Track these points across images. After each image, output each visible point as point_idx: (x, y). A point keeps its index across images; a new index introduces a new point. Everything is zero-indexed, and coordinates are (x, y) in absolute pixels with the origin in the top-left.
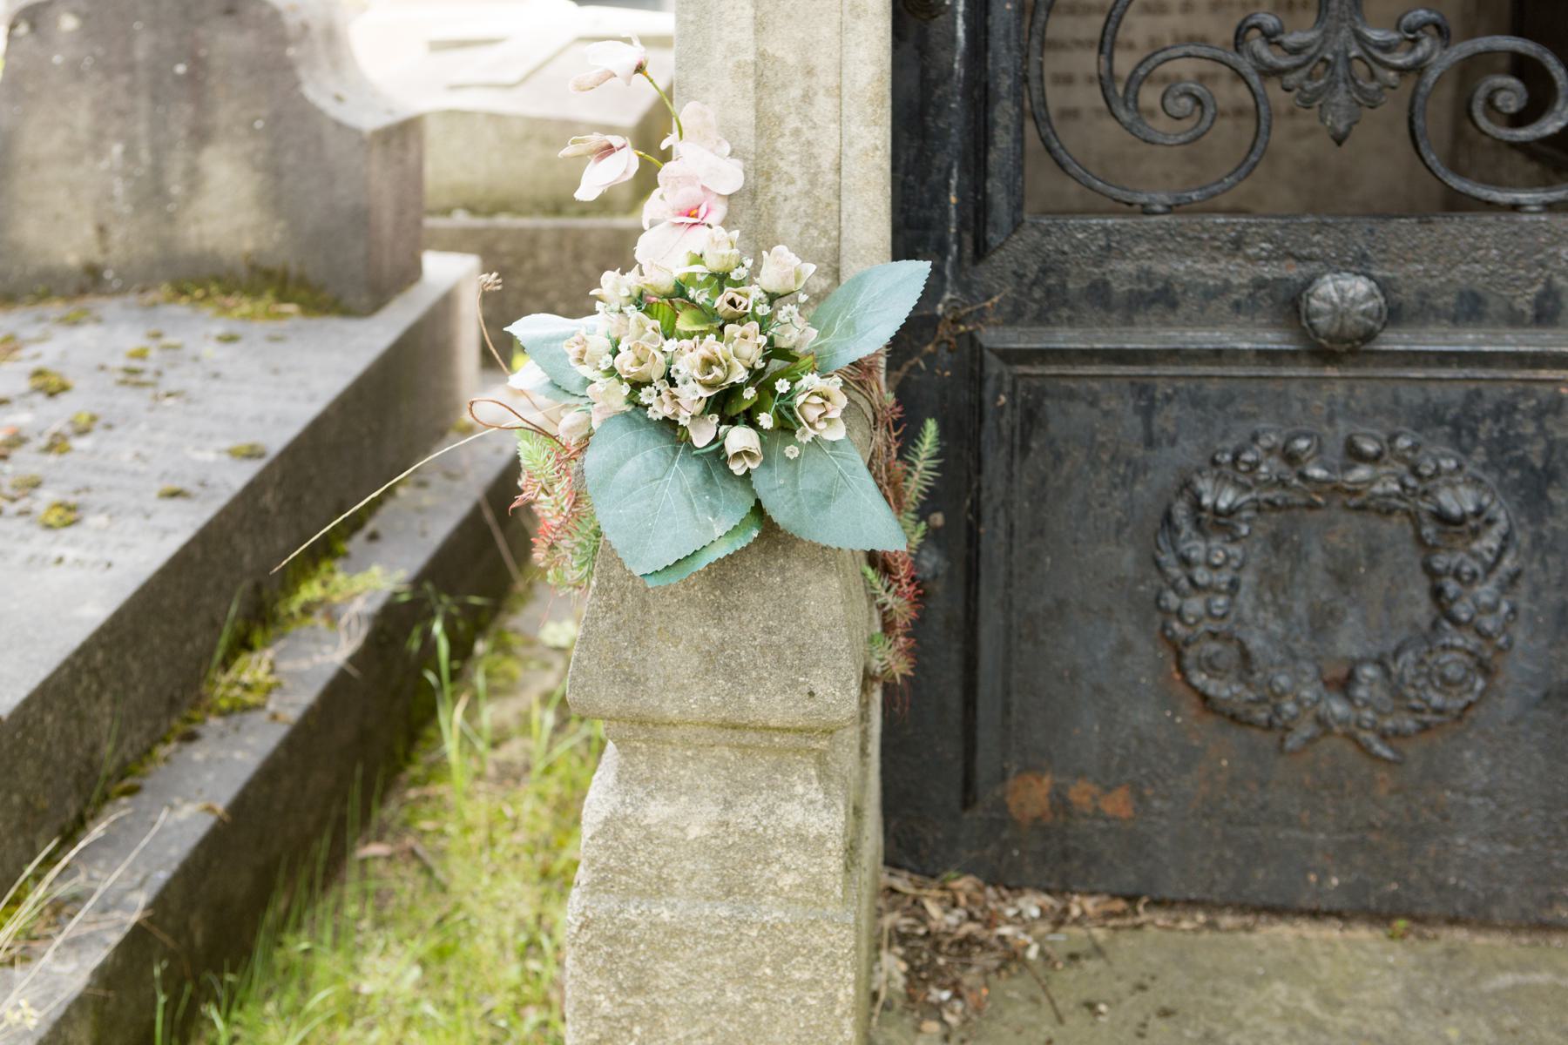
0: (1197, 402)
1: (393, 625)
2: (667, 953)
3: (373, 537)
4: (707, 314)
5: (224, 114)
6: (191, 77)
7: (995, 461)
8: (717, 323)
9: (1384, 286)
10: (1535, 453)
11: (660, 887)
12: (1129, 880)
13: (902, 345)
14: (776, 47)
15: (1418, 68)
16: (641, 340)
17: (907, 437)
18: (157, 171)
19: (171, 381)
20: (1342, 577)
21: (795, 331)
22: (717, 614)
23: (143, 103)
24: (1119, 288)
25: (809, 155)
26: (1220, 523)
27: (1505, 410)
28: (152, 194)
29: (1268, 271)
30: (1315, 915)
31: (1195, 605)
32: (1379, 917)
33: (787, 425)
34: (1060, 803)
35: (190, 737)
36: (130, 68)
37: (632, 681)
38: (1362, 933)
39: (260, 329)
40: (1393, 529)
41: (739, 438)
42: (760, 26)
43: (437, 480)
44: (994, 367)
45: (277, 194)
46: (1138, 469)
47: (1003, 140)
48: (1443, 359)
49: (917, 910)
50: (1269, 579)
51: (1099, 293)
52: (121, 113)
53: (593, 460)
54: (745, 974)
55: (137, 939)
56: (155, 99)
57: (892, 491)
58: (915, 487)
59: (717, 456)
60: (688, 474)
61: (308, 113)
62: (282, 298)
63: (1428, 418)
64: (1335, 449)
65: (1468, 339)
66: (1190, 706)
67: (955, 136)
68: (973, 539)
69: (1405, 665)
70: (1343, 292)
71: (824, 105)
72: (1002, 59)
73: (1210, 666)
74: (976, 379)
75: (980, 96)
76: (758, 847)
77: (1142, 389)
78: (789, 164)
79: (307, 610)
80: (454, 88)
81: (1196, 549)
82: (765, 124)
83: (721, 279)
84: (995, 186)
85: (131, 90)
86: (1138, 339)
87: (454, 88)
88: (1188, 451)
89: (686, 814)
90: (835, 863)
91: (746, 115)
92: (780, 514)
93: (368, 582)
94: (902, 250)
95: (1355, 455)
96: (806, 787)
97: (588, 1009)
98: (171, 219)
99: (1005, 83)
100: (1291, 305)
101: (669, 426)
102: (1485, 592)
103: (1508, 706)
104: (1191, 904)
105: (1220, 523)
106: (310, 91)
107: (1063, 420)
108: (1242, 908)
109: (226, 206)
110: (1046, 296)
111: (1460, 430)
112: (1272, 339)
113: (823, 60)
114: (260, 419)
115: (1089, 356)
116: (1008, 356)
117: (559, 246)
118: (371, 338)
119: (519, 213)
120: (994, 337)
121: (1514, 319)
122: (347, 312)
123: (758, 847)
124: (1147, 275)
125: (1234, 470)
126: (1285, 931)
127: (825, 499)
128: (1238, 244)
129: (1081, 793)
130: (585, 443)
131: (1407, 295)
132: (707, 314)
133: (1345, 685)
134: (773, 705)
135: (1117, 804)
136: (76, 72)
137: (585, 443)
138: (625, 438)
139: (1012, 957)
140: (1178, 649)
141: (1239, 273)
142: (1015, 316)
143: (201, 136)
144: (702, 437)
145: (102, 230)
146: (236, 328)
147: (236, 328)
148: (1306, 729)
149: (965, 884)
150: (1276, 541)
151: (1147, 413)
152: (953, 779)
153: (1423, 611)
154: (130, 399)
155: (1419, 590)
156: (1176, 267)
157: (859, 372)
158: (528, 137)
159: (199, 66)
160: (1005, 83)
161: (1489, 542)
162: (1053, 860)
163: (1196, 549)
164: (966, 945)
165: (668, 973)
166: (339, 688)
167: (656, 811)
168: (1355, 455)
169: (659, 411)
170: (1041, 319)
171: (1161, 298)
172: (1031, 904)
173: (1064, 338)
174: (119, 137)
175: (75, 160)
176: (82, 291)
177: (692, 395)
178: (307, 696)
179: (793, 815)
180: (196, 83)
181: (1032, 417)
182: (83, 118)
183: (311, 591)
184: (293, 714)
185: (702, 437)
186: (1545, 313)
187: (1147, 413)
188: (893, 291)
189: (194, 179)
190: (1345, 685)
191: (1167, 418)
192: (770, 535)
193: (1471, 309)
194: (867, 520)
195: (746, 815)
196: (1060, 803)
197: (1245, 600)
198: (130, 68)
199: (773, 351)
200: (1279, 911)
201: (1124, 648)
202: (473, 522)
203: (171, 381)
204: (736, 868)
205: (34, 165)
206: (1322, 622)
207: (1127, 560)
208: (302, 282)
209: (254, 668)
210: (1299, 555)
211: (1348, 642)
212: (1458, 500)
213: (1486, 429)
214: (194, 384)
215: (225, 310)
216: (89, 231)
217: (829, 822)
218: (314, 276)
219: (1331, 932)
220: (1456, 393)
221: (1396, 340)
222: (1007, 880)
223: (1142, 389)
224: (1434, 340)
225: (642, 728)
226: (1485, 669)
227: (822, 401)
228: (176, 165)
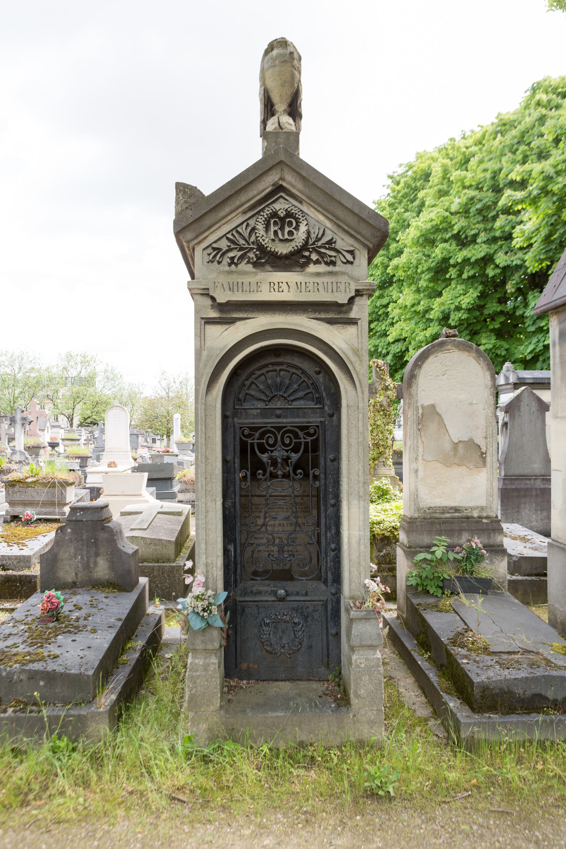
0: (264, 607)
1: (144, 651)
2: (198, 678)
3: (136, 636)
4: (201, 599)
5: (102, 550)
6: (94, 542)
7: (239, 617)
8: (203, 600)
9: (286, 591)
10: (306, 613)
11: (197, 671)
12: (257, 678)
13: (225, 601)
14: (209, 561)
15: (291, 560)
16: (194, 603)
17: (226, 614)
18: (88, 562)
19: (100, 606)
20: (283, 632)
21: (212, 600)
22: (203, 636)
23: (85, 547)
24: (254, 591)
25: (213, 576)
26: (267, 625)
27: (302, 608)
28: (87, 567)
29: (273, 589)
30: (281, 681)
31: (265, 637)
32: (289, 680)
33: (211, 612)
34: (249, 667)
35: (118, 668)
36: (82, 540)
37: (194, 645)
38: (287, 683)
39: (111, 595)
40: (289, 625)
41: (206, 614)
42: (206, 558)
43: (145, 625)
44: (238, 603)
45: (112, 567)
46: (257, 617)
47: (239, 570)
48: (294, 601)
49: (229, 683)
50: (274, 633)
51: (252, 592)
52: (80, 550)
53: (189, 617)
54: (207, 680)
55: (120, 693)
56: (87, 547)
57: (223, 621)
58: (227, 620)
59: (203, 616)
60: (199, 619)
61: (119, 550)
62: (114, 588)
63: (293, 609)
64: (282, 615)
65: (297, 598)
66: (265, 652)
67: (232, 569)
68: (236, 629)
69: (290, 644)
70: (282, 592)
71: (214, 568)
72: (238, 558)
73: (267, 645)
74: (236, 605)
75: (235, 564)
76: (208, 665)
77: (257, 606)
78: (210, 577)
79: (129, 648)
80: (132, 530)
81: (265, 628)
82: (207, 571)
83: (203, 595)
84: (238, 577)
85: (82, 545)
86: (257, 599)
87: (132, 530)
88: (263, 615)
89: (200, 661)
90: (217, 666)
91: (205, 570)
92: (210, 623)
93: (139, 643)
94: (225, 590)
95: (284, 615)
96: (214, 657)
97: (189, 686)
98: (91, 572)
99: (239, 562)
100: (275, 593)
101: (197, 613)
102: (300, 633)
103: (303, 649)
104: (265, 680)
105: (267, 625)
106: (119, 546)
107: (247, 610)
108: (272, 680)
109: (102, 569)
110: (245, 593)
111: (297, 611)
112: (273, 599)
113: (214, 562)
114: (119, 613)
115: (250, 601)
116: (240, 602)
117: (159, 570)
118: (133, 597)
119: (149, 562)
120: (239, 599)
121: (303, 595)
122: (127, 591)
123: (208, 665)
124: (257, 590)
125: (269, 617)
126: (277, 683)
127: (215, 621)
128: (269, 585)
129: (251, 665)
130: (188, 615)
131: (290, 592)
132: (201, 599)
133: (283, 647)
134: (210, 647)
135: (256, 666)
136: (71, 540)
137: (188, 615)
138: (192, 614)
139: (242, 688)
140: (263, 643)
141: (269, 589)
142: (241, 596)
143: (97, 555)
144: (201, 614)
145: (76, 574)
146: (107, 595)
147: (107, 595)
148: (279, 654)
149: (236, 680)
150: (275, 627)
151: (258, 609)
152: (236, 665)
153: (293, 636)
154: (94, 610)
155: (293, 633)
156: (261, 588)
157: (219, 606)
158: (151, 544)
159: (96, 539)
160: (239, 562)
161: (300, 626)
162: (248, 675)
163: (265, 628)
164: (236, 687)
165: (198, 681)
166: (138, 659)
167: (196, 661)
168: (284, 615)
169: (196, 611)
170: (244, 596)
171: (259, 593)
172: (245, 682)
173: (247, 599)
174: (80, 555)
175: (71, 559)
176: (72, 587)
177: (200, 609)
178: (134, 662)
179: (212, 660)
180: (96, 543)
181: (243, 610)
182: (72, 551)
183: (129, 645)
184: (133, 664)
185: (201, 614)
186: (306, 594)
187: (258, 609)
188: (223, 595)
189: (96, 563)
190: (283, 647)
191: (261, 610)
192: (209, 625)
193: (297, 594)
194: (219, 623)
195: (207, 661)
196: (249, 667)
197: (271, 636)
198: (82, 540)
199: (209, 603)
200: (277, 680)
201: (256, 643)
202: (153, 633)
203: (100, 606)
204: (206, 668)
205: (62, 560)
206: (281, 638)
207: (256, 630)
208: (118, 585)
209: (124, 657)
210: (278, 629)
211: (284, 641)
212: (296, 620)
213: (300, 611)
214: (104, 607)
215: (103, 591)
216: (74, 574)
217: (216, 661)
218: (120, 584)
219: (283, 683)
220: (296, 606)
221: (289, 598)
222: (241, 679)
223: (257, 606)
224: (293, 598)
225: (194, 650)
226: (301, 644)
227: (214, 608)
228: (92, 560)
